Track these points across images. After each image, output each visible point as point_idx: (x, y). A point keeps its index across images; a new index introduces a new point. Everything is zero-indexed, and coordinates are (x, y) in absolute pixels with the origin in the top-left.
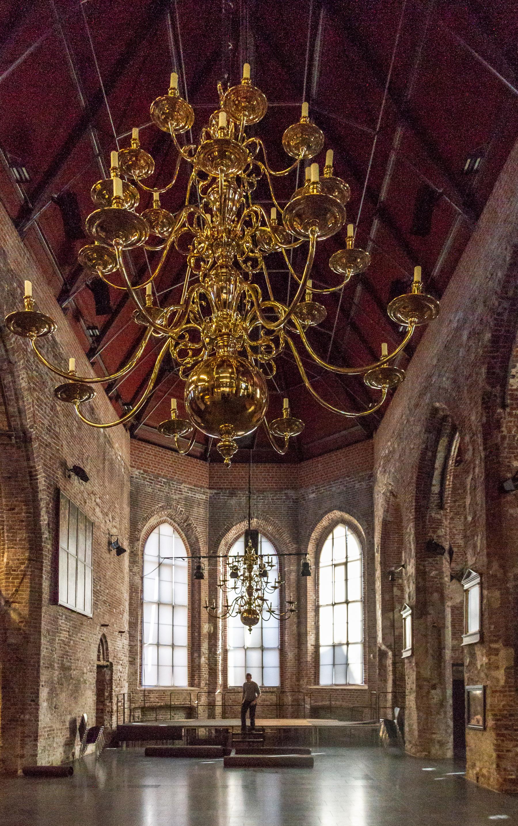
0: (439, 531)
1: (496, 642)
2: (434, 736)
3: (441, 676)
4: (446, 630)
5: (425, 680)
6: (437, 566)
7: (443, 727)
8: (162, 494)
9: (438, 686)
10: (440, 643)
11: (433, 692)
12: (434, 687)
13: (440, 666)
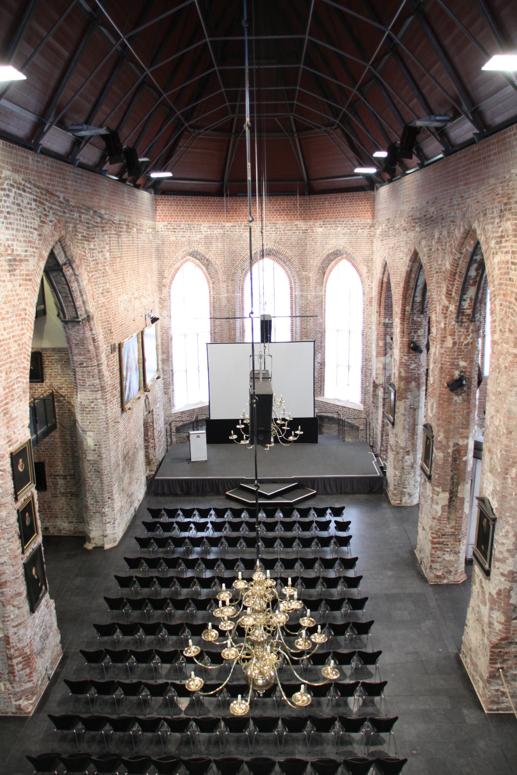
0: (419, 331)
1: (438, 486)
2: (405, 490)
3: (414, 445)
4: (420, 410)
5: (401, 448)
6: (417, 360)
7: (412, 482)
8: (184, 239)
9: (411, 454)
10: (414, 420)
11: (407, 457)
12: (408, 453)
13: (413, 438)
